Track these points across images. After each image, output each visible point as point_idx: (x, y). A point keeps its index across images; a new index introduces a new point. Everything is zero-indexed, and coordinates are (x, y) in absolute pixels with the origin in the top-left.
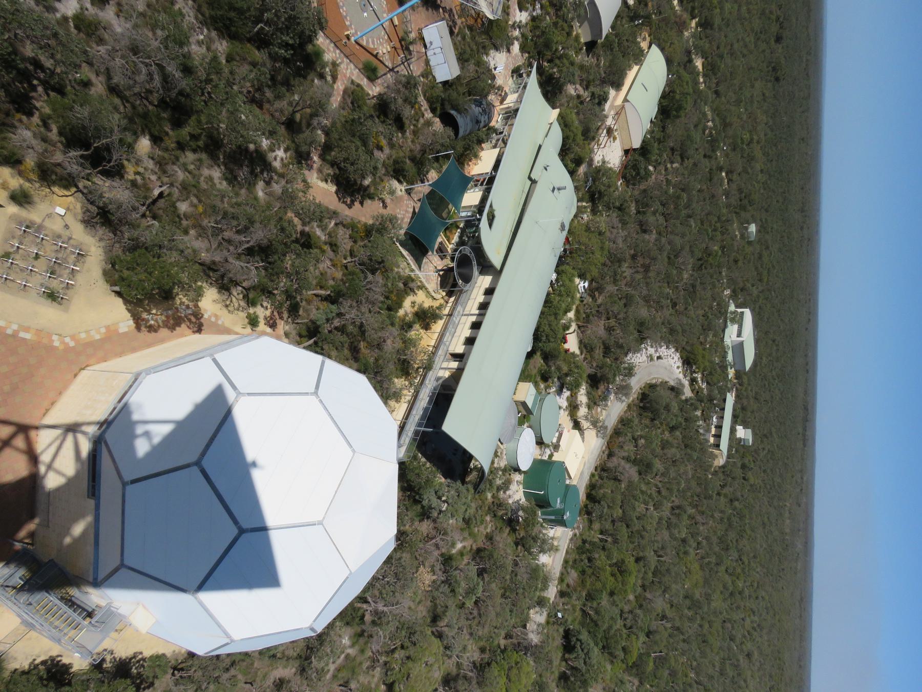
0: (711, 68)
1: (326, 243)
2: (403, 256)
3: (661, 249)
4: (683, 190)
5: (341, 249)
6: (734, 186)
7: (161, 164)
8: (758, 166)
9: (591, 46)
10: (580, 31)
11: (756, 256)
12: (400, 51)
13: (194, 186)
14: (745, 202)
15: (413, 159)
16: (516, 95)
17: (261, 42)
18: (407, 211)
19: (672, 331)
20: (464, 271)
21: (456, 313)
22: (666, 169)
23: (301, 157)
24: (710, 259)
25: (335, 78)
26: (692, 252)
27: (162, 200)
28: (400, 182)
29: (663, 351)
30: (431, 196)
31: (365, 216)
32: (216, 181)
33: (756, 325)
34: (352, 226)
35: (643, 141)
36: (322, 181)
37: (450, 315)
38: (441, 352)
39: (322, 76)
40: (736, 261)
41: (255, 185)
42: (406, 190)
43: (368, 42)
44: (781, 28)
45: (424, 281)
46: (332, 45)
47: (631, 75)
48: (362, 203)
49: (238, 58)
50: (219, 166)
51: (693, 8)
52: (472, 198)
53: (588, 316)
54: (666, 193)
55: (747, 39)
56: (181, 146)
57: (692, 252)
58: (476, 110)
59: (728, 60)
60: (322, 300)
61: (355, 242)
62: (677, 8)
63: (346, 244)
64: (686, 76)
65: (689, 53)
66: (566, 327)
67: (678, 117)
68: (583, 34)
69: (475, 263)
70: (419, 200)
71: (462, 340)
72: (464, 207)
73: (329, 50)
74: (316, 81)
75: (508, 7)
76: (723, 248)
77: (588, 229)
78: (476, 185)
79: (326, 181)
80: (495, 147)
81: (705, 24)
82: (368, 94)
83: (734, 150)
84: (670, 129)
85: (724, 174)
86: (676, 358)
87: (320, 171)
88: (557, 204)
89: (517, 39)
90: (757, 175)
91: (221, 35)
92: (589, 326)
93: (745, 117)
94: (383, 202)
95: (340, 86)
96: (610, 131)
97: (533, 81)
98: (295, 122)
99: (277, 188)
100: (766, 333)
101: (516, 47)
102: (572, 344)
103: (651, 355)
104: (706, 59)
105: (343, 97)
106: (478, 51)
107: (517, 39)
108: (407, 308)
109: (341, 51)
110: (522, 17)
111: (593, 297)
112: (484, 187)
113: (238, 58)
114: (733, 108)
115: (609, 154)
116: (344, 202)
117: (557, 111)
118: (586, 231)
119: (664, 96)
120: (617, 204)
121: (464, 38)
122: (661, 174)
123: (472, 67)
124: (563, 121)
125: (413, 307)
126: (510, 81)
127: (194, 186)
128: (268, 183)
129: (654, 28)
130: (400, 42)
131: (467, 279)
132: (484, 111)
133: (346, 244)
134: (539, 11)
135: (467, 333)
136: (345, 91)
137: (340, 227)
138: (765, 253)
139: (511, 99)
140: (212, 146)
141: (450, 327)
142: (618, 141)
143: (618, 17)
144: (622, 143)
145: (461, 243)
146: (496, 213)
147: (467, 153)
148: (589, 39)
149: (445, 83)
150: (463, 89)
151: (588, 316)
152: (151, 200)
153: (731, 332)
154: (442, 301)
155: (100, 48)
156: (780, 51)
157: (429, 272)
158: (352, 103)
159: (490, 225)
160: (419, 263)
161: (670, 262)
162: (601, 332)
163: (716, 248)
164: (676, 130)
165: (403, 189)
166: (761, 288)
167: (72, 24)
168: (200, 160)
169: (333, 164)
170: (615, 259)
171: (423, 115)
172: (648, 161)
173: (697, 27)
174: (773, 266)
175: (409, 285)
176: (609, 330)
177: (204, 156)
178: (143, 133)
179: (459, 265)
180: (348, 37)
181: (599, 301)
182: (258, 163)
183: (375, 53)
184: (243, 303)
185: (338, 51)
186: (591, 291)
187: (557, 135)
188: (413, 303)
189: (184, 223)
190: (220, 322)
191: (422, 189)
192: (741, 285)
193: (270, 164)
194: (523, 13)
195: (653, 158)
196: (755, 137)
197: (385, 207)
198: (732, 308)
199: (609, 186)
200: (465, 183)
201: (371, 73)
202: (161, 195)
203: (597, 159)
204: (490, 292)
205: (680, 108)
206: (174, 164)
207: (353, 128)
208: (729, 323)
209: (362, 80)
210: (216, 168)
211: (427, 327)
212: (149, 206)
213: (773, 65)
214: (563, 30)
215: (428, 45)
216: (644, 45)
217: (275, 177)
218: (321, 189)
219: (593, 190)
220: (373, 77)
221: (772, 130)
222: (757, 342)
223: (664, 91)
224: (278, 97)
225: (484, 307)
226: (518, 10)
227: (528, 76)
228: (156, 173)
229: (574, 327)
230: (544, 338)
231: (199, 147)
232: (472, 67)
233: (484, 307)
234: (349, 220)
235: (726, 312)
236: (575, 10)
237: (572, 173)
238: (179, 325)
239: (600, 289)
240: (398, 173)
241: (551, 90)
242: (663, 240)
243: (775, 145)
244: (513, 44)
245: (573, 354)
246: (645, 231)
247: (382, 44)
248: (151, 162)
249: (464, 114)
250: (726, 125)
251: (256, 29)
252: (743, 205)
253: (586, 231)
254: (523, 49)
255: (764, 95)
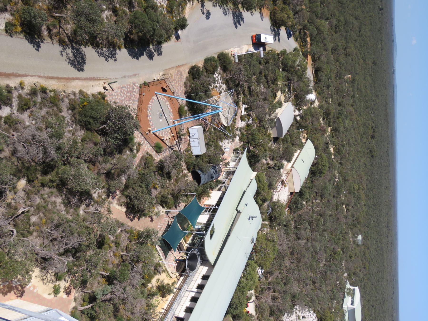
0: (338, 151)
1: (113, 242)
2: (157, 251)
3: (307, 250)
4: (321, 215)
5: (121, 245)
6: (350, 214)
7: (28, 194)
8: (363, 203)
9: (276, 139)
10: (271, 132)
11: (362, 253)
12: (176, 138)
13: (44, 207)
14: (356, 222)
15: (173, 195)
16: (234, 163)
17: (103, 133)
18: (164, 224)
19: (312, 300)
20: (191, 263)
21: (183, 290)
22: (313, 203)
23: (110, 193)
24: (336, 256)
25: (138, 151)
26: (325, 251)
27: (23, 215)
28: (163, 207)
29: (306, 314)
30: (179, 215)
31: (139, 226)
32: (58, 204)
33: (362, 297)
34: (130, 232)
35: (301, 189)
36: (119, 205)
37: (179, 289)
38: (169, 316)
39: (131, 150)
40: (351, 257)
41: (80, 206)
42: (166, 212)
43: (159, 133)
44: (374, 132)
45: (166, 266)
46: (140, 134)
47: (296, 155)
48: (139, 219)
49: (88, 140)
50: (62, 196)
51: (330, 122)
52: (203, 218)
53: (262, 291)
54: (312, 217)
55: (357, 138)
56: (43, 185)
57: (325, 251)
58: (212, 171)
59: (347, 148)
60: (102, 277)
61: (130, 241)
62: (321, 122)
63: (124, 242)
64: (324, 156)
65: (327, 144)
66: (249, 299)
67: (320, 177)
68: (273, 133)
69: (199, 258)
70: (173, 218)
71: (184, 308)
72: (198, 223)
73: (138, 136)
74: (128, 152)
75: (235, 119)
76: (343, 249)
77: (267, 239)
78: (206, 211)
79: (121, 205)
80: (219, 190)
81: (335, 130)
82: (155, 160)
83: (350, 193)
84: (316, 182)
85: (344, 206)
86: (314, 317)
87: (119, 200)
88: (250, 225)
89: (238, 135)
90: (362, 208)
91: (82, 127)
92: (262, 297)
93: (356, 177)
94: (152, 218)
95: (140, 155)
96: (283, 182)
97: (244, 157)
98: (111, 173)
99: (92, 209)
100: (369, 301)
101: (237, 139)
102: (251, 308)
103: (298, 316)
104: (336, 146)
105: (141, 161)
106: (217, 140)
107: (238, 135)
108: (154, 283)
109: (144, 138)
110: (241, 124)
111: (266, 278)
112: (210, 213)
113: (88, 140)
114: (349, 172)
115: (281, 195)
116: (129, 218)
117: (255, 173)
118: (266, 239)
119: (314, 165)
120: (284, 223)
121: (210, 134)
122: (310, 206)
123: (212, 149)
124: (258, 179)
125: (157, 282)
126: (232, 155)
127: (44, 207)
128: (88, 206)
129: (309, 131)
130: (177, 134)
131: (193, 268)
132: (216, 172)
133: (124, 242)
134: (251, 121)
135: (188, 303)
136: (142, 158)
137: (124, 232)
138: (367, 252)
139: (232, 165)
140: (62, 185)
141: (178, 298)
142: (287, 188)
143: (292, 125)
144: (289, 188)
145: (193, 245)
146: (215, 230)
147: (203, 193)
148: (276, 136)
149: (197, 156)
150: (206, 159)
151: (262, 291)
152: (16, 216)
153: (348, 300)
154: (176, 279)
155: (14, 133)
156: (374, 142)
157: (170, 261)
158: (145, 164)
159: (211, 236)
160: (166, 254)
161: (313, 258)
162: (270, 301)
163: (339, 250)
164: (319, 182)
165: (164, 211)
166: (365, 273)
167: (3, 120)
168: (52, 193)
169: (127, 197)
170: (280, 256)
171: (182, 171)
172: (303, 199)
173: (331, 131)
174: (372, 259)
175: (158, 268)
176: (274, 299)
177: (54, 190)
178: (24, 177)
179: (190, 259)
180: (149, 131)
181: (270, 280)
182: (85, 196)
183: (162, 139)
184: (53, 278)
185: (143, 137)
186: (266, 274)
187: (254, 187)
188: (158, 280)
189: (32, 228)
190: (35, 291)
191: (175, 212)
192: (354, 271)
193: (91, 196)
194: (243, 122)
195: (306, 197)
196: (361, 187)
197: (152, 221)
198: (348, 286)
199: (280, 215)
200: (200, 210)
201: (158, 149)
202: (23, 213)
203: (275, 198)
204: (206, 278)
205: (321, 173)
206: (36, 194)
207: (143, 179)
208: (346, 295)
209: (153, 152)
210: (60, 197)
211: (163, 296)
212: (14, 218)
213: (370, 149)
214: (262, 132)
215: (191, 135)
216: (304, 141)
217: (92, 203)
218: (117, 210)
219: (272, 216)
220: (159, 151)
221: (370, 183)
222: (363, 308)
223: (313, 162)
224: (105, 162)
225: (201, 287)
226: (240, 120)
227: (242, 153)
228: (24, 199)
229: (253, 298)
230: (234, 307)
231: (53, 186)
232: (212, 149)
233: (201, 287)
234: (129, 228)
235: (345, 289)
236: (270, 123)
237: (260, 206)
238: (9, 291)
239: (271, 273)
240: (163, 202)
241: (253, 160)
242: (309, 244)
243: (372, 191)
244: (236, 137)
245: (251, 315)
246: (299, 238)
247: (167, 135)
248: (23, 192)
249: (205, 172)
250: (345, 180)
251: (102, 127)
252: (355, 225)
253: (266, 239)
254: (240, 140)
255: (365, 164)
